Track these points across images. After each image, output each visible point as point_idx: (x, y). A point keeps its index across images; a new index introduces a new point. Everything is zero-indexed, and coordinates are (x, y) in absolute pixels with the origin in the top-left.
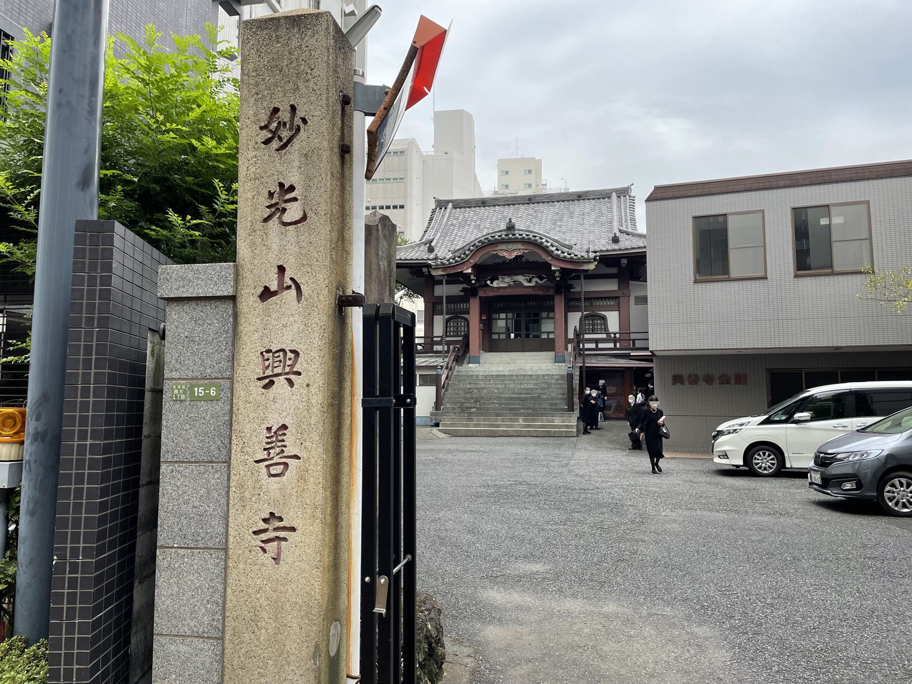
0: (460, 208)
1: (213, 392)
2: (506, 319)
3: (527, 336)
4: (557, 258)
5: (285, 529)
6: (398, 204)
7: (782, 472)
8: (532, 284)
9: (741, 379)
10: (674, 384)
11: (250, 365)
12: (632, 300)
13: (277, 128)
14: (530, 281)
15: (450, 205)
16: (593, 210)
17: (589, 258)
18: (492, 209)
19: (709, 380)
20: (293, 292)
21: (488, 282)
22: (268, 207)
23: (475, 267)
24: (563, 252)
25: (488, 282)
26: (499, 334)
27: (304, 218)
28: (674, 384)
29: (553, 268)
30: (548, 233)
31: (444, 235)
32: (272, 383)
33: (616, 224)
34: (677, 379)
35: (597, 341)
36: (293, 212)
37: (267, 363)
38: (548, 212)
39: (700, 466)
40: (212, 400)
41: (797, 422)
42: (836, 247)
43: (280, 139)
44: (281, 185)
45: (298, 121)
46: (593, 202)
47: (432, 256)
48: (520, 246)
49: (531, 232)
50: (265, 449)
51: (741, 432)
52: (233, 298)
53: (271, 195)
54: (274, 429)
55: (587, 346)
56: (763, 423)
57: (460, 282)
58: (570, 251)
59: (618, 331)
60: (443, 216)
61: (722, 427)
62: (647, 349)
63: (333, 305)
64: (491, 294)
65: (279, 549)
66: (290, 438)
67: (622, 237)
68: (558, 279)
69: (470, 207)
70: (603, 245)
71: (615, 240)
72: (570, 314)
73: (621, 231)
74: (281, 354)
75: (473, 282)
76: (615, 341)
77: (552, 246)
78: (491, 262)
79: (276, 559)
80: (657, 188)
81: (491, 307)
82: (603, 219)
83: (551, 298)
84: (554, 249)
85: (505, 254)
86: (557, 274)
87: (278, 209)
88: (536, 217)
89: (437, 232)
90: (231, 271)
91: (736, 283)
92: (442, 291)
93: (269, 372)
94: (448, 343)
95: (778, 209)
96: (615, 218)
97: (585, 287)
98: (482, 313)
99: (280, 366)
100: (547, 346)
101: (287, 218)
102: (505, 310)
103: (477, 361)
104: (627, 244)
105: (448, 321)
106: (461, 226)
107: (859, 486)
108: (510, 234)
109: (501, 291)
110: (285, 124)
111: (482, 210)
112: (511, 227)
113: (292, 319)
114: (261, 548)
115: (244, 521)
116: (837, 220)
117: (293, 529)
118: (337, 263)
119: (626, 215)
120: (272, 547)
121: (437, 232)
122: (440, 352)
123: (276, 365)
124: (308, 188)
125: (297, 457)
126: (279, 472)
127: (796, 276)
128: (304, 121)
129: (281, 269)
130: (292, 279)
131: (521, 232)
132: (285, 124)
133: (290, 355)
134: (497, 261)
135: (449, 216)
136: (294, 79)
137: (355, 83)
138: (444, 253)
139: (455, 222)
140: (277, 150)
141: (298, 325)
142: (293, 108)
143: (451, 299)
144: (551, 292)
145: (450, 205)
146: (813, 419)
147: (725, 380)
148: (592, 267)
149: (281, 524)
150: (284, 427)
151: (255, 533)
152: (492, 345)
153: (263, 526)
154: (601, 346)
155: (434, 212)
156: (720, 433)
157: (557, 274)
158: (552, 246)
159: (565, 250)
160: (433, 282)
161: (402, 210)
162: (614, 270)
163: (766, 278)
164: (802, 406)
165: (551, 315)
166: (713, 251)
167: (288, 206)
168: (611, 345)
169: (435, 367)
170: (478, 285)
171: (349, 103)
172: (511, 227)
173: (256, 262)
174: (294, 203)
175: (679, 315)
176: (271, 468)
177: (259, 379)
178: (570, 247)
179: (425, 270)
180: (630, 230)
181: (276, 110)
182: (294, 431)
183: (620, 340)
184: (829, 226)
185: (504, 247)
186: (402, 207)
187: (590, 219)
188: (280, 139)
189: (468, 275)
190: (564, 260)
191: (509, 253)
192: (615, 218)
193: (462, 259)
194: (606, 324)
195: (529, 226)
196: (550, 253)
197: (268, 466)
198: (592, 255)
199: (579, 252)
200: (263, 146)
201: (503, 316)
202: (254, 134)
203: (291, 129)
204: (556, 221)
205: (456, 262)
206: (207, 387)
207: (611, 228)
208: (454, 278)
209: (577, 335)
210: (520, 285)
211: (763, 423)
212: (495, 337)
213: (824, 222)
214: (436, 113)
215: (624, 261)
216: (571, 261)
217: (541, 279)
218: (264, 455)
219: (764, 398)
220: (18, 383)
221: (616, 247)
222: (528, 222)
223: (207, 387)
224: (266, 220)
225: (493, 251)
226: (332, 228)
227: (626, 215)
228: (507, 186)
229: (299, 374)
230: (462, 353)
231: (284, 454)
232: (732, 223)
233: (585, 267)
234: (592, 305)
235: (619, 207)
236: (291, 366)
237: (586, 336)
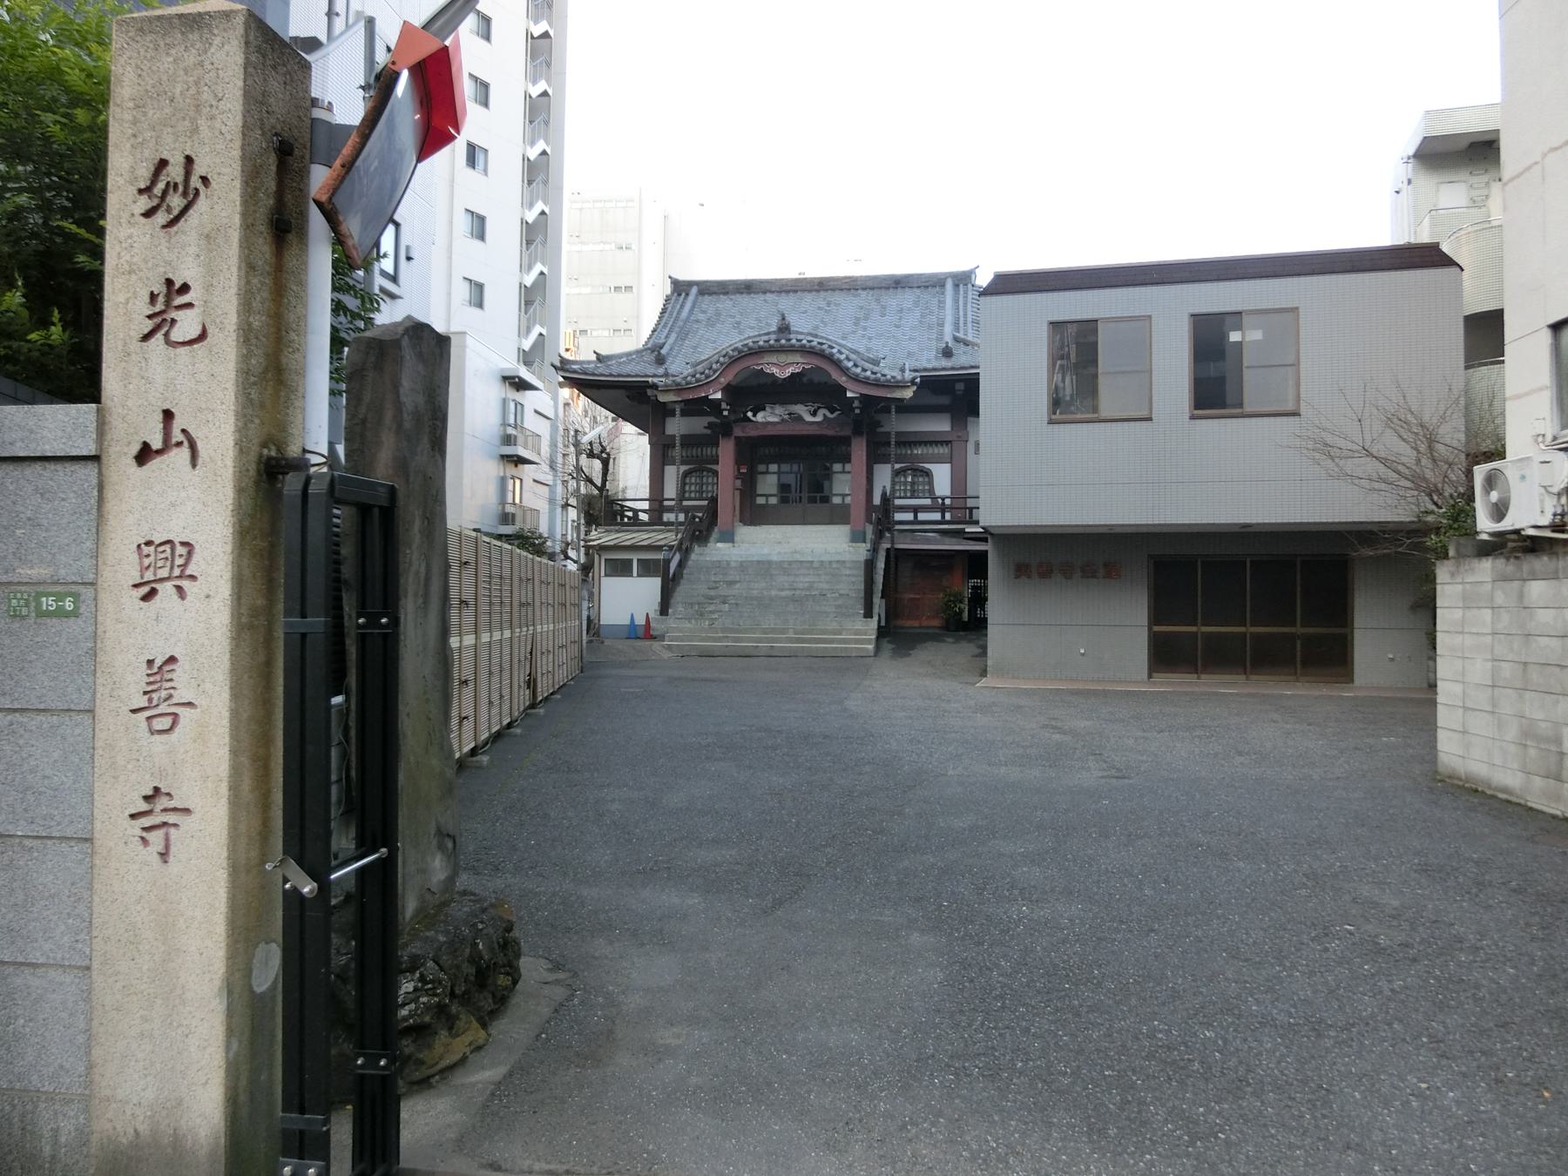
1: (69, 605)
2: (779, 473)
3: (809, 500)
4: (856, 379)
5: (175, 810)
8: (819, 418)
10: (1017, 577)
13: (165, 192)
14: (814, 414)
15: (694, 290)
16: (916, 304)
17: (903, 381)
18: (762, 297)
20: (185, 452)
21: (750, 414)
22: (149, 317)
23: (727, 389)
24: (864, 370)
25: (750, 414)
26: (767, 496)
27: (202, 336)
28: (1017, 577)
29: (849, 394)
30: (844, 338)
32: (152, 593)
33: (948, 329)
34: (1021, 571)
35: (916, 510)
37: (146, 562)
38: (848, 305)
40: (68, 615)
42: (1245, 371)
43: (169, 210)
44: (169, 282)
45: (195, 182)
46: (918, 291)
47: (661, 371)
48: (798, 358)
49: (816, 336)
50: (145, 693)
52: (96, 458)
53: (153, 297)
54: (158, 663)
55: (898, 516)
57: (701, 413)
58: (876, 369)
60: (682, 306)
62: (977, 523)
63: (252, 473)
64: (754, 433)
65: (167, 839)
66: (180, 674)
67: (959, 350)
70: (928, 360)
71: (947, 353)
72: (876, 467)
73: (956, 339)
74: (167, 548)
76: (943, 509)
77: (848, 359)
79: (164, 855)
81: (755, 452)
83: (846, 441)
84: (850, 364)
85: (775, 370)
86: (856, 404)
87: (164, 320)
89: (670, 331)
90: (93, 417)
92: (676, 426)
93: (149, 576)
94: (686, 510)
95: (1170, 318)
97: (897, 425)
98: (739, 461)
99: (165, 568)
100: (839, 516)
101: (177, 334)
102: (779, 459)
103: (729, 537)
105: (686, 474)
106: (711, 323)
110: (176, 185)
113: (183, 494)
114: (142, 838)
117: (187, 811)
118: (262, 406)
119: (965, 315)
120: (156, 837)
122: (672, 524)
123: (160, 564)
124: (209, 287)
125: (190, 704)
126: (167, 727)
127: (1193, 417)
128: (205, 180)
129: (168, 415)
130: (183, 431)
132: (176, 185)
133: (180, 550)
136: (192, 113)
137: (313, 120)
138: (680, 367)
139: (701, 317)
140: (164, 227)
141: (195, 507)
142: (189, 160)
143: (689, 441)
144: (847, 432)
145: (694, 290)
148: (908, 394)
149: (172, 804)
150: (172, 660)
151: (133, 816)
152: (754, 514)
153: (144, 807)
154: (922, 516)
157: (856, 404)
158: (848, 359)
159: (867, 365)
160: (665, 411)
161: (628, 295)
162: (944, 400)
163: (1150, 419)
165: (848, 467)
167: (178, 315)
168: (937, 516)
169: (659, 548)
170: (733, 418)
171: (290, 154)
172: (784, 329)
173: (130, 403)
174: (188, 312)
175: (1024, 470)
176: (155, 721)
177: (135, 586)
178: (876, 362)
179: (649, 392)
180: (970, 338)
181: (163, 164)
182: (187, 667)
183: (951, 508)
184: (1240, 344)
185: (773, 359)
186: (629, 288)
188: (169, 210)
189: (717, 402)
190: (866, 382)
194: (931, 483)
195: (817, 327)
197: (149, 718)
198: (908, 375)
199: (889, 371)
200: (143, 220)
201: (773, 467)
202: (129, 201)
203: (185, 194)
204: (858, 319)
206: (60, 597)
207: (941, 334)
208: (696, 407)
209: (886, 500)
210: (800, 419)
212: (761, 501)
213: (1235, 337)
216: (877, 384)
218: (143, 702)
221: (945, 363)
222: (806, 322)
223: (60, 597)
224: (146, 337)
226: (250, 351)
227: (965, 315)
229: (193, 577)
230: (702, 528)
231: (174, 701)
233: (898, 394)
235: (956, 301)
236: (185, 565)
237: (898, 502)
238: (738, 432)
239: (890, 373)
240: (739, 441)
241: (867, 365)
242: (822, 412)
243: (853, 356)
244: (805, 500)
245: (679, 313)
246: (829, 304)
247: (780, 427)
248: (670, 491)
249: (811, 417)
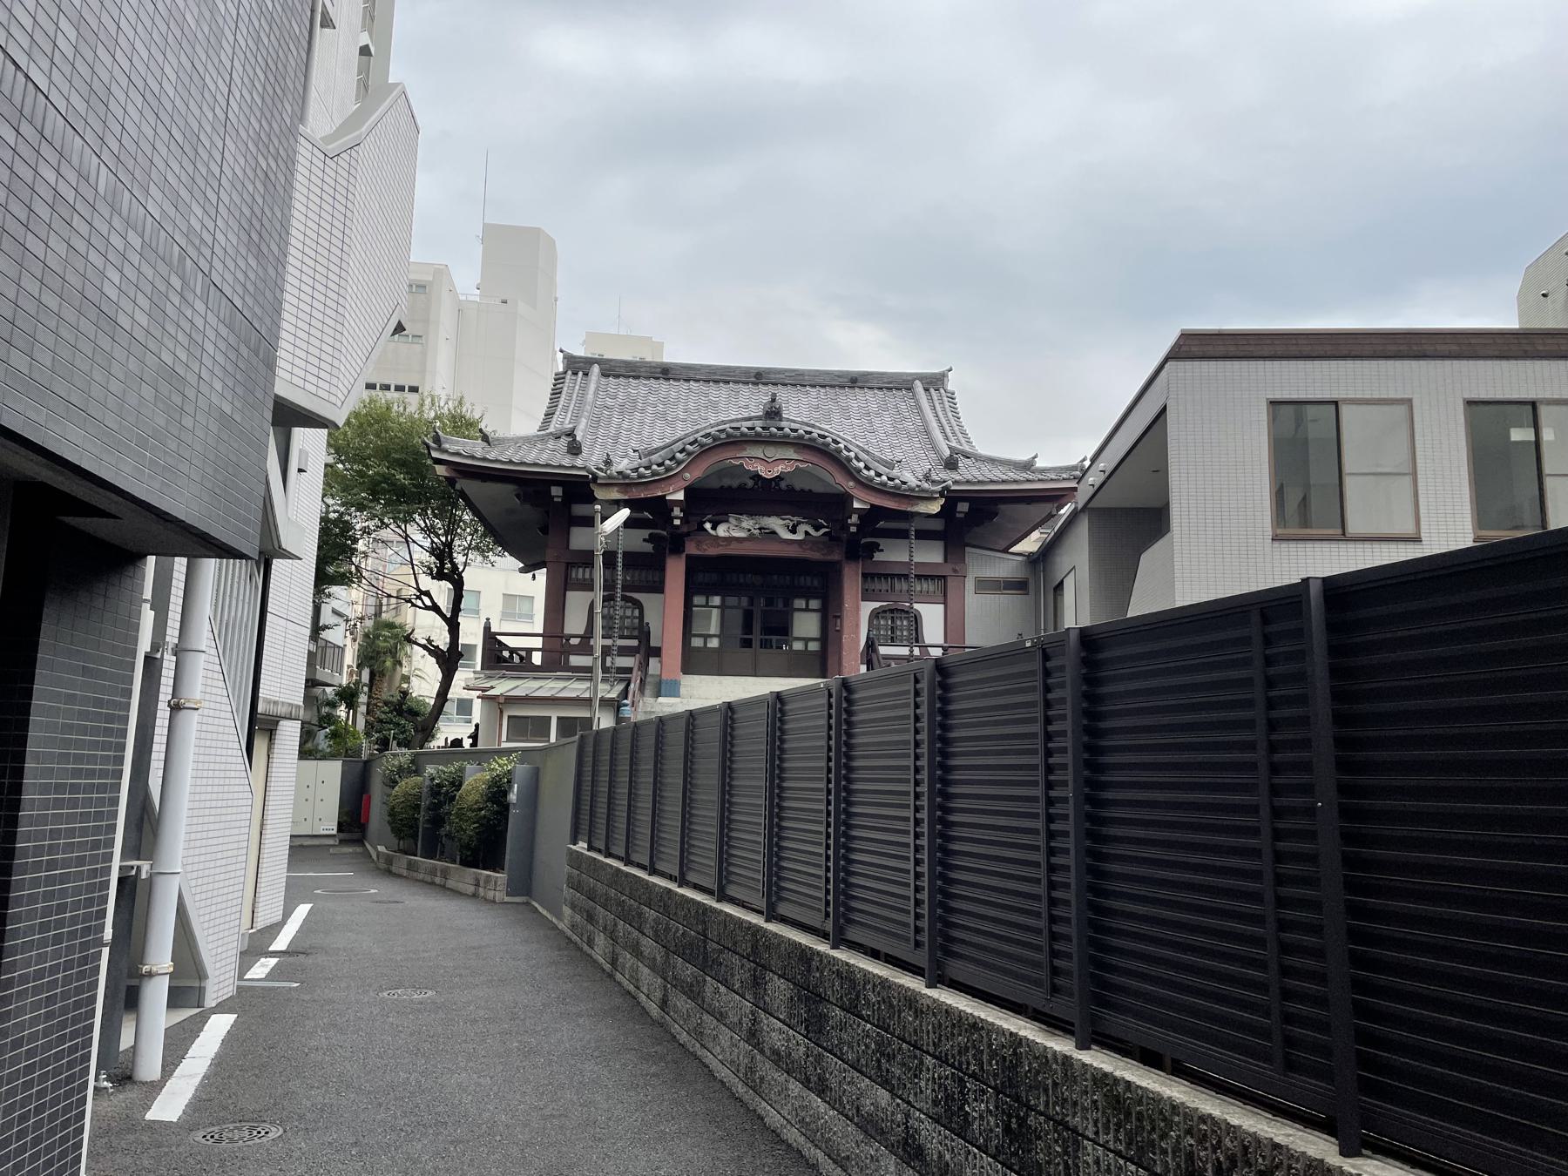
0: (617, 376)
4: (867, 485)
6: (407, 382)
8: (799, 536)
12: (970, 585)
18: (685, 385)
21: (708, 526)
23: (689, 491)
24: (879, 475)
25: (708, 526)
31: (596, 423)
38: (857, 400)
48: (790, 453)
58: (895, 472)
59: (941, 641)
60: (584, 388)
64: (712, 551)
68: (853, 529)
69: (635, 377)
71: (951, 464)
75: (677, 522)
77: (858, 460)
78: (715, 484)
80: (1186, 337)
86: (854, 519)
91: (1359, 545)
108: (770, 432)
109: (734, 545)
111: (663, 386)
131: (794, 426)
134: (726, 482)
135: (597, 389)
145: (596, 369)
155: (559, 378)
178: (890, 465)
185: (757, 452)
190: (881, 490)
191: (770, 465)
193: (668, 469)
196: (852, 474)
205: (654, 474)
214: (487, 228)
217: (817, 528)
220: (110, 718)
222: (799, 411)
225: (732, 458)
234: (893, 588)
238: (691, 549)
239: (913, 482)
240: (691, 561)
241: (882, 469)
242: (802, 528)
243: (862, 455)
244: (756, 643)
247: (747, 545)
248: (575, 624)
249: (786, 532)
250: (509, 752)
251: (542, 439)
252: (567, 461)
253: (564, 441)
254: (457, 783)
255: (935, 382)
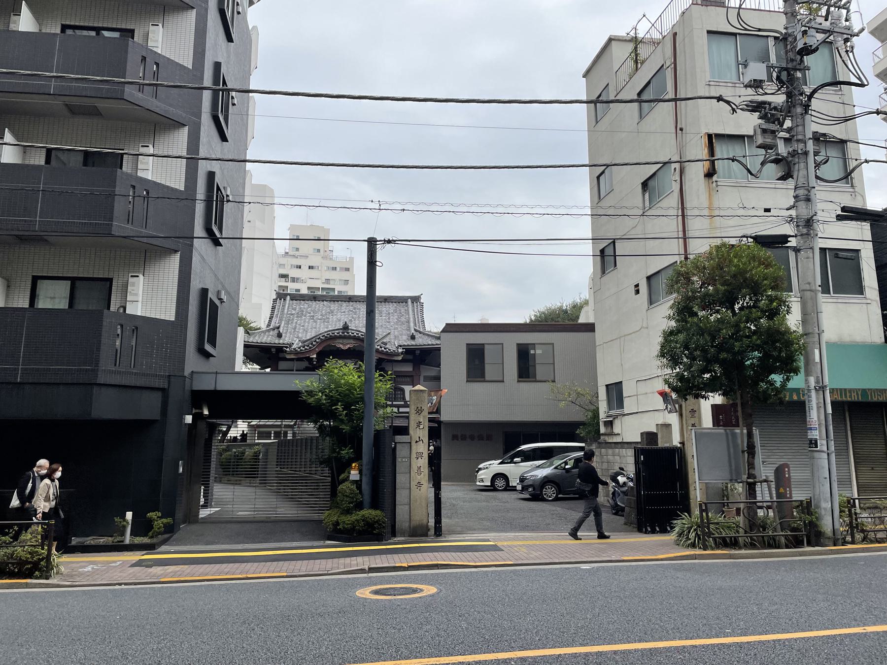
7: (508, 488)
9: (489, 438)
11: (414, 456)
18: (322, 303)
19: (472, 438)
23: (317, 354)
31: (288, 323)
34: (455, 437)
36: (421, 427)
39: (472, 488)
41: (515, 463)
48: (352, 341)
51: (490, 468)
56: (500, 463)
60: (284, 306)
61: (481, 466)
67: (417, 335)
70: (405, 341)
71: (413, 337)
73: (415, 330)
80: (447, 324)
82: (403, 319)
88: (355, 313)
89: (281, 320)
95: (511, 342)
96: (412, 319)
99: (419, 455)
104: (421, 341)
107: (534, 489)
111: (314, 304)
112: (346, 327)
115: (413, 484)
116: (539, 352)
121: (281, 320)
139: (293, 312)
145: (288, 298)
146: (522, 461)
147: (481, 438)
154: (401, 410)
155: (275, 301)
156: (480, 469)
164: (517, 455)
166: (476, 363)
172: (346, 327)
187: (394, 319)
190: (382, 353)
191: (344, 346)
192: (412, 319)
199: (391, 348)
207: (409, 329)
211: (500, 463)
213: (532, 352)
215: (418, 352)
216: (387, 354)
219: (501, 447)
221: (413, 343)
228: (297, 249)
232: (487, 348)
245: (284, 309)
246: (355, 308)
250: (258, 444)
251: (268, 331)
252: (277, 341)
253: (276, 331)
254: (243, 453)
255: (416, 299)
